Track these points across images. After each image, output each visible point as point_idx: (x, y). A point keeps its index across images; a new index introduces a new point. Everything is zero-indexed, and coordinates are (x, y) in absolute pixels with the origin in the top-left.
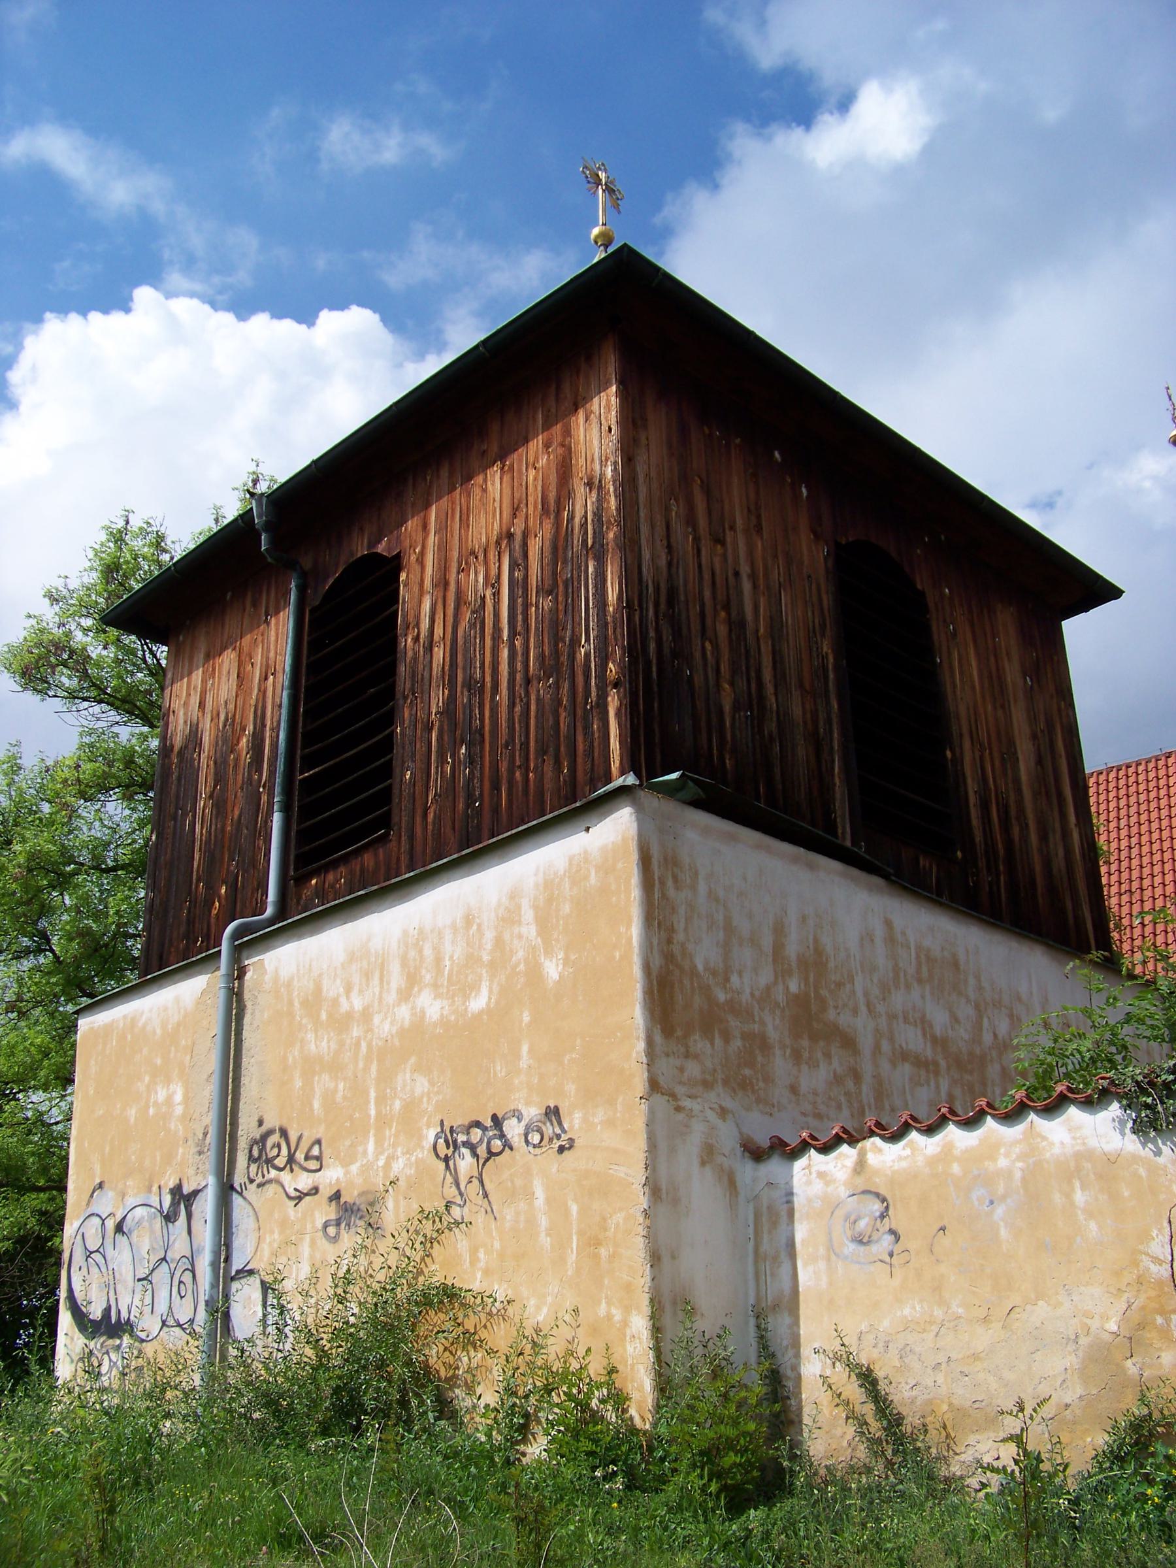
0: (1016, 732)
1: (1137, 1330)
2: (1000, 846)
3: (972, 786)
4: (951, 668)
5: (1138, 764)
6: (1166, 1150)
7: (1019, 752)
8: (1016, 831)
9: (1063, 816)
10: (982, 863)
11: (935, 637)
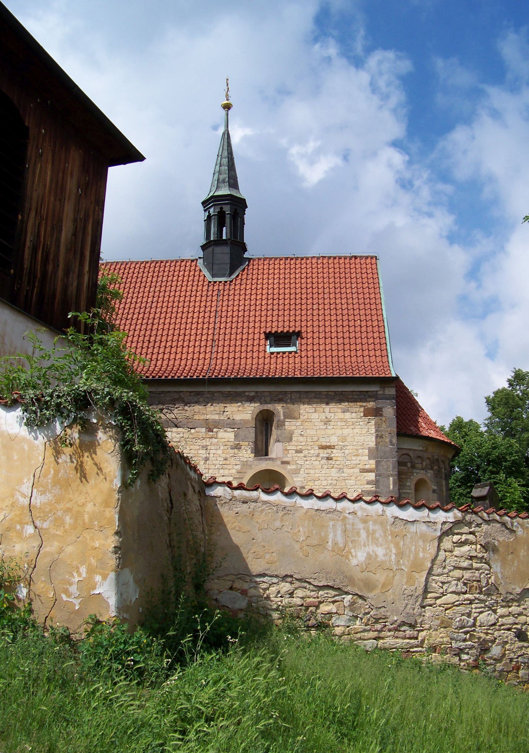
0: (65, 216)
1: (6, 531)
2: (39, 272)
3: (29, 238)
4: (34, 173)
5: (167, 262)
6: (40, 437)
7: (64, 225)
8: (50, 267)
9: (82, 265)
10: (25, 279)
11: (29, 153)
